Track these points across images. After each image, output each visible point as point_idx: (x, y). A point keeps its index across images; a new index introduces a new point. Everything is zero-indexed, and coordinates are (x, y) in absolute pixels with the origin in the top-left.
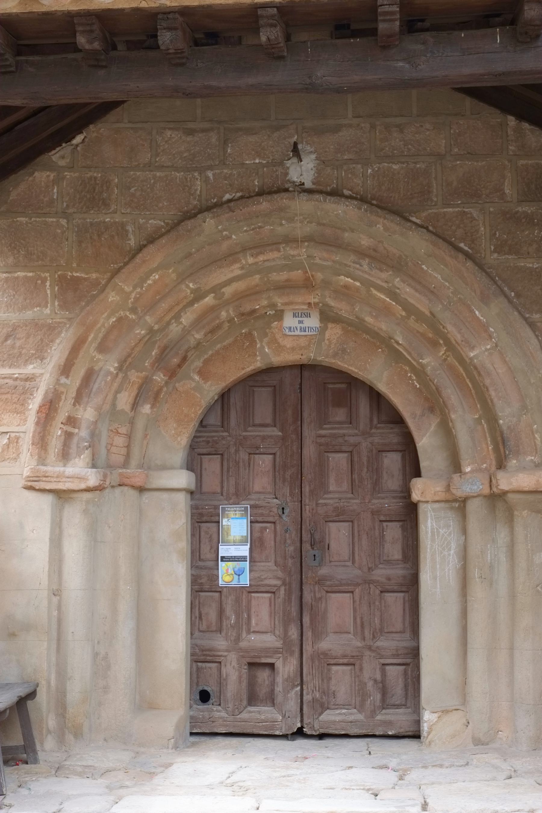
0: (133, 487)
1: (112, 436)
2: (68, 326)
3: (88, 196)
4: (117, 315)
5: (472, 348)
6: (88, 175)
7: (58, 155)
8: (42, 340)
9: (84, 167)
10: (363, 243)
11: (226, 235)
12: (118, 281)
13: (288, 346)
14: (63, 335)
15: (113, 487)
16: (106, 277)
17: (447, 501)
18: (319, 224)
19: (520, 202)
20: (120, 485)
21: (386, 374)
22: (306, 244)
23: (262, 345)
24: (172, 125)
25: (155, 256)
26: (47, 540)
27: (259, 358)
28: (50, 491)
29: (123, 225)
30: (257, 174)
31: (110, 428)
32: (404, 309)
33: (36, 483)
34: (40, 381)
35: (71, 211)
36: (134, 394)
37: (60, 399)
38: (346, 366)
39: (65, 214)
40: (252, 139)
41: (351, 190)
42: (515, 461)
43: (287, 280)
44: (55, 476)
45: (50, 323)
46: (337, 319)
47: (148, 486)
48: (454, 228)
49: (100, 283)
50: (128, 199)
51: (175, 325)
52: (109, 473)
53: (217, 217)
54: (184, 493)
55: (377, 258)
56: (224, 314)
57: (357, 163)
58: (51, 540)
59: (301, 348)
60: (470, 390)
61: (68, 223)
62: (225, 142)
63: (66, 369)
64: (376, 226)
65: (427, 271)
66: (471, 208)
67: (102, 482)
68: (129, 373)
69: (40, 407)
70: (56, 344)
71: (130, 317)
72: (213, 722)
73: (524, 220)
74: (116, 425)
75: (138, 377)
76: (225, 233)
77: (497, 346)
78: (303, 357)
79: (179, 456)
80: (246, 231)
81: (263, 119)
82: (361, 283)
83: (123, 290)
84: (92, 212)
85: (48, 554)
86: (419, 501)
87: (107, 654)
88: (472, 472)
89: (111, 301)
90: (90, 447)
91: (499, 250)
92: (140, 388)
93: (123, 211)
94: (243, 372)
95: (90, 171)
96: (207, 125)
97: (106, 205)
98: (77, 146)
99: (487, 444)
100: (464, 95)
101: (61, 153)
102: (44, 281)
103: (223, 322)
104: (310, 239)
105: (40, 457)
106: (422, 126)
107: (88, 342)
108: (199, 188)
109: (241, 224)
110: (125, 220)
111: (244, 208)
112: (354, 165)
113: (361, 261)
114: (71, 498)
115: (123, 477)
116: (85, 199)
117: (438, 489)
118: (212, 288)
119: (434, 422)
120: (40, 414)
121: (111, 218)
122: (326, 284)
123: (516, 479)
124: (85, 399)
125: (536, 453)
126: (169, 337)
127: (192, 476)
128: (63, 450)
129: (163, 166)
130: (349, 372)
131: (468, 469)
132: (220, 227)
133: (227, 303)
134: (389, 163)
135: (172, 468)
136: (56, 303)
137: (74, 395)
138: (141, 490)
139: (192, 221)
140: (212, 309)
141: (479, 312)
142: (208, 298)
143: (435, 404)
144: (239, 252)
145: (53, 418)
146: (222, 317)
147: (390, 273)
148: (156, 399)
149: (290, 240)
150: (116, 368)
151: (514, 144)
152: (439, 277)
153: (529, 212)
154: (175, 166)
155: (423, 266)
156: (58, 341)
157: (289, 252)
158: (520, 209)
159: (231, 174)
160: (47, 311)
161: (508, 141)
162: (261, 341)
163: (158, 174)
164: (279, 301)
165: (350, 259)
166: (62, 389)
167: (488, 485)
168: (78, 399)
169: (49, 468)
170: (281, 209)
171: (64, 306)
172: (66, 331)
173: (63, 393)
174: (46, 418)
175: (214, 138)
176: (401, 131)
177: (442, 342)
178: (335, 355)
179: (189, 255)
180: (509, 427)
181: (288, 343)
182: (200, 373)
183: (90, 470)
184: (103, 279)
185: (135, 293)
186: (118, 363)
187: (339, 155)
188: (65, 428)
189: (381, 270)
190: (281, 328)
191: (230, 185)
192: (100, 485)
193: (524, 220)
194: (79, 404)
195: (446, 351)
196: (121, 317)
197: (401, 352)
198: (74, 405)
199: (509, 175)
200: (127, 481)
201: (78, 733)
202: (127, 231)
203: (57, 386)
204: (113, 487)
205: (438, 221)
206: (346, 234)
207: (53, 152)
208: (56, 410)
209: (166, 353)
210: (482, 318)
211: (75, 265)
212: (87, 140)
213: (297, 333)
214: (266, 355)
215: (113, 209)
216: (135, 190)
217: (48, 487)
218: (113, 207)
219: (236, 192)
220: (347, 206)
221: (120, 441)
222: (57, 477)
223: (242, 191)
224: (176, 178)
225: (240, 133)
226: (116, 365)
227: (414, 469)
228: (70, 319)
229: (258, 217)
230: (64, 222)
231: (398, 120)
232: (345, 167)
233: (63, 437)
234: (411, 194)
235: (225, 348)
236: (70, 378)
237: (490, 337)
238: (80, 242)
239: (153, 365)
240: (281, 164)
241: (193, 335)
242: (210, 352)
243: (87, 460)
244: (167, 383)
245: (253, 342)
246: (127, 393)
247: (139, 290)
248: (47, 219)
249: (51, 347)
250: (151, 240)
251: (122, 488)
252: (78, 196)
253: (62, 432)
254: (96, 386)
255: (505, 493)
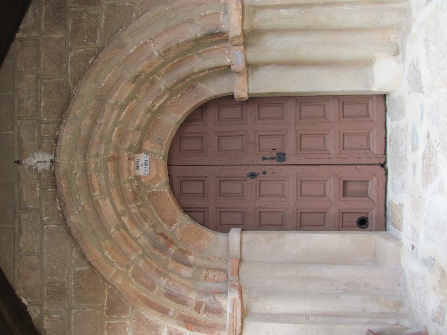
0: (239, 267)
1: (208, 280)
2: (137, 310)
3: (58, 295)
4: (130, 278)
5: (153, 54)
6: (46, 295)
7: (33, 314)
8: (146, 326)
9: (41, 298)
10: (88, 123)
11: (81, 208)
12: (108, 277)
13: (156, 172)
14: (143, 313)
15: (239, 279)
16: (107, 285)
17: (248, 76)
18: (75, 150)
19: (66, 28)
20: (238, 275)
21: (172, 114)
22: (87, 158)
23: (155, 188)
24: (17, 242)
25: (93, 253)
26: (274, 324)
27: (163, 190)
28: (242, 323)
29: (76, 274)
30: (45, 189)
31: (203, 280)
32: (132, 100)
33: (237, 332)
34: (172, 328)
35: (67, 306)
36: (182, 266)
37: (183, 315)
38: (167, 138)
39: (69, 310)
40: (25, 192)
41: (56, 131)
42: (223, 26)
43: (115, 172)
44: (232, 319)
45: (136, 321)
46: (141, 144)
47: (239, 258)
48: (80, 68)
49: (111, 289)
50: (60, 270)
51: (140, 240)
52: (231, 283)
53: (68, 214)
54: (243, 235)
55: (97, 114)
56: (133, 210)
57: (40, 127)
58: (274, 322)
59: (157, 165)
60: (181, 60)
61: (75, 309)
62: (27, 209)
63: (164, 311)
64: (77, 115)
65: (105, 83)
66: (68, 57)
67: (237, 288)
68: (169, 269)
69: (188, 329)
70: (149, 317)
71: (132, 269)
72: (379, 217)
73: (77, 26)
74: (202, 277)
75: (172, 263)
76: (80, 209)
77: (151, 39)
78: (162, 164)
79: (221, 237)
80: (79, 196)
81: (14, 186)
82: (116, 127)
83: (114, 275)
84: (68, 293)
85: (283, 324)
86: (248, 93)
87: (344, 284)
88: (230, 59)
89: (122, 282)
90: (214, 296)
91: (93, 39)
92: (179, 262)
93: (67, 274)
94: (171, 199)
95: (43, 294)
96: (17, 221)
97: (63, 284)
98: (29, 302)
99: (213, 49)
100: (3, 64)
101: (32, 311)
102: (109, 324)
103: (139, 211)
104: (85, 156)
105: (220, 329)
106: (20, 89)
107: (148, 297)
108: (53, 225)
109: (74, 199)
110: (72, 273)
111: (63, 197)
112: (42, 129)
113: (98, 124)
114: (247, 308)
115: (233, 273)
116: (60, 297)
117: (240, 81)
118: (118, 217)
119: (201, 86)
120: (193, 329)
121: (71, 281)
122: (117, 148)
123: (233, 24)
124: (184, 298)
125: (218, 13)
126: (148, 244)
127: (247, 99)
128: (216, 313)
129: (40, 248)
130: (172, 138)
131: (229, 60)
132: (76, 212)
133: (127, 208)
134: (41, 108)
135: (228, 242)
136: (123, 316)
137: (181, 306)
138: (241, 261)
139: (71, 230)
140: (131, 218)
141: (131, 50)
142: (124, 220)
143: (188, 83)
144: (92, 200)
145: (196, 320)
146: (136, 211)
147: (106, 105)
148: (185, 252)
149: (85, 170)
150: (164, 279)
151: (32, 33)
152: (109, 75)
153: (72, 23)
154: (40, 240)
155: (102, 85)
156: (147, 316)
157: (92, 169)
158: (70, 28)
159: (45, 206)
160: (128, 322)
161: (30, 37)
162: (153, 188)
163: (45, 251)
164: (126, 176)
165: (98, 131)
166: (177, 314)
167: (238, 47)
168: (183, 302)
169: (228, 323)
170: (66, 173)
171: (125, 311)
172: (141, 311)
173: (179, 313)
174: (195, 325)
175: (24, 216)
176: (22, 101)
177: (152, 77)
178: (161, 144)
179: (94, 232)
180: (202, 30)
181: (154, 173)
182: (171, 225)
183: (228, 297)
184: (108, 287)
185: (117, 266)
186: (161, 277)
187: (35, 138)
188: (202, 311)
189: (104, 111)
190: (145, 177)
191: (52, 206)
192: (239, 289)
193: (77, 26)
194: (187, 302)
195: (157, 75)
196: (132, 275)
197: (160, 106)
198: (187, 306)
199: (50, 35)
200: (236, 271)
201: (400, 304)
202: (79, 271)
203: (175, 317)
204: (239, 279)
205: (76, 77)
206: (83, 133)
207: (32, 317)
208: (190, 318)
209: (157, 246)
210: (134, 48)
211: (100, 305)
212: (25, 296)
213: (149, 167)
214: (161, 185)
215: (66, 280)
216: (55, 266)
217: (239, 324)
218: (65, 280)
219: (56, 202)
220: (63, 132)
221: (211, 275)
222: (233, 318)
223: (55, 199)
224: (47, 240)
225: (21, 200)
226: (162, 278)
227: (228, 99)
228: (133, 309)
229: (70, 189)
230: (74, 311)
231: (16, 103)
232: (42, 135)
233: (208, 313)
234: (59, 94)
235: (157, 210)
236: (170, 309)
237: (146, 43)
238: (86, 301)
239: (164, 254)
240: (39, 174)
241: (146, 229)
242: (159, 219)
243: (222, 298)
244: (176, 246)
245: (153, 193)
246: (182, 271)
247: (115, 264)
248: (72, 322)
249: (151, 320)
250: (84, 256)
251: (240, 274)
252: (58, 302)
253: (205, 314)
254: (175, 291)
255: (243, 32)
